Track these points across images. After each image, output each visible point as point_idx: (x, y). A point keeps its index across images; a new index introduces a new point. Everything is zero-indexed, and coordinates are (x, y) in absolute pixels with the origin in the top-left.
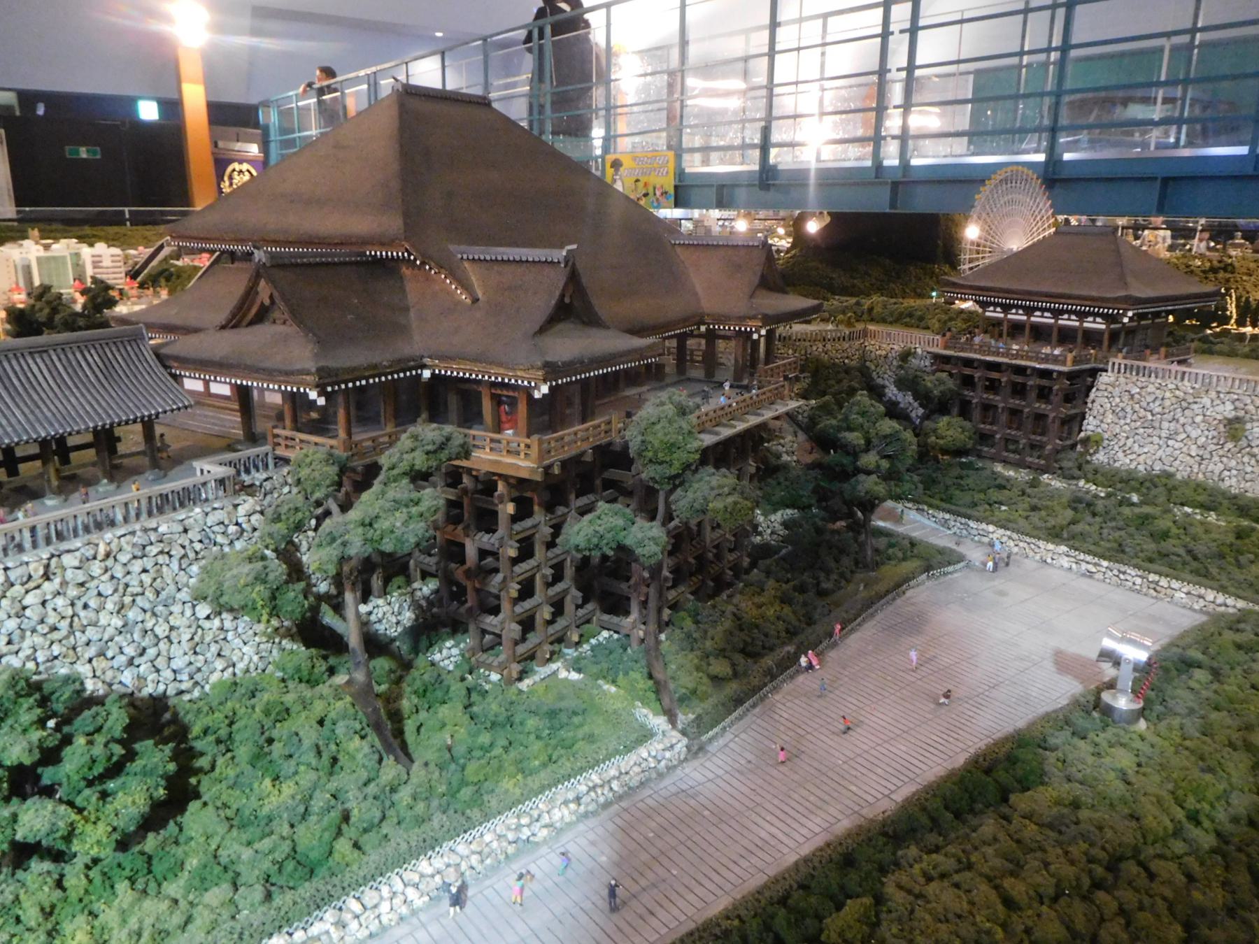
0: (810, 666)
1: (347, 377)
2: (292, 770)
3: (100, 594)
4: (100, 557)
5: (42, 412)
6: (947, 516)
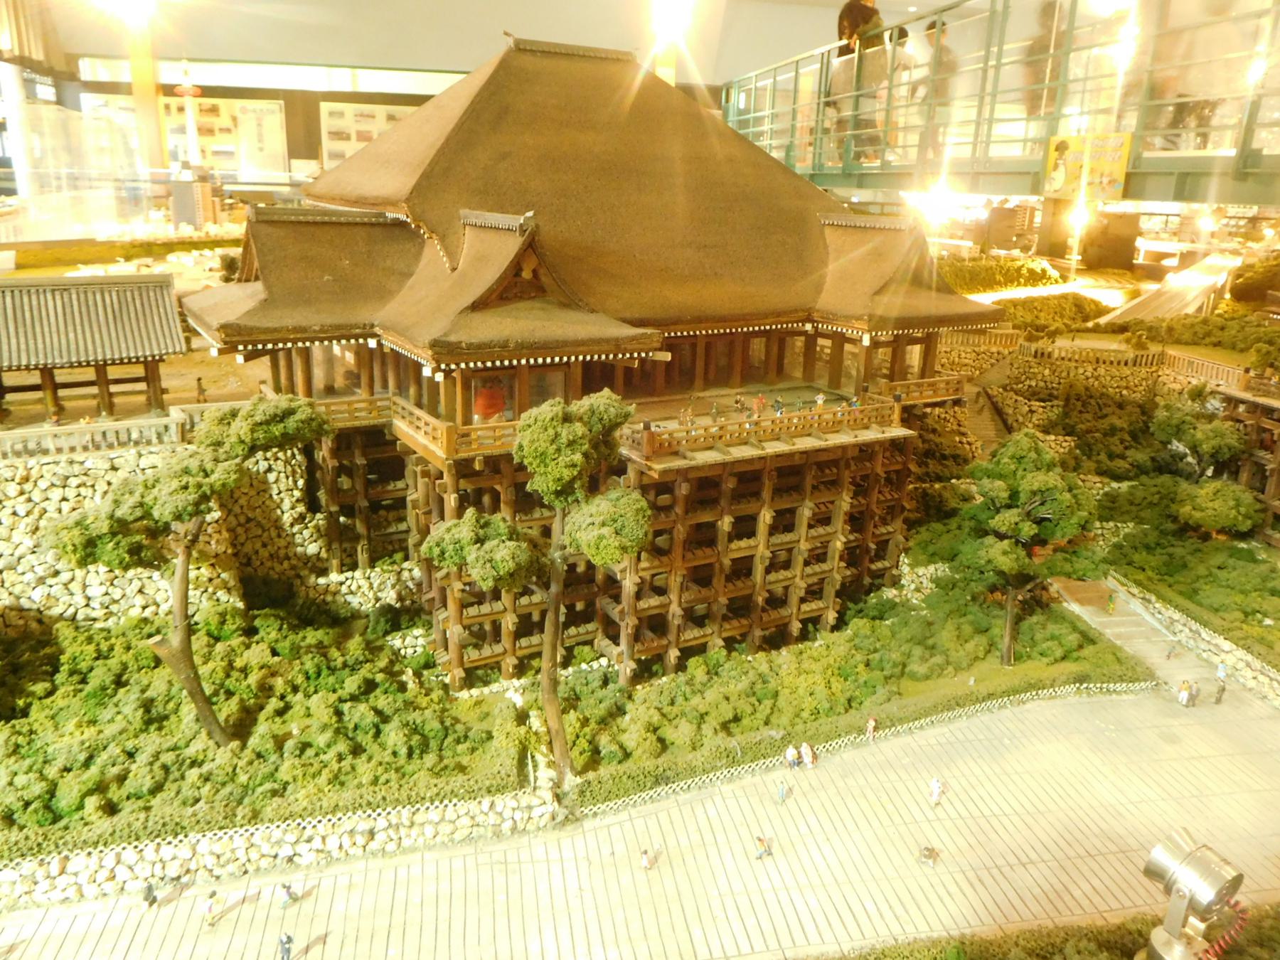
0: (799, 762)
1: (263, 337)
2: (109, 717)
3: (15, 514)
4: (17, 480)
5: (36, 344)
6: (1177, 616)
